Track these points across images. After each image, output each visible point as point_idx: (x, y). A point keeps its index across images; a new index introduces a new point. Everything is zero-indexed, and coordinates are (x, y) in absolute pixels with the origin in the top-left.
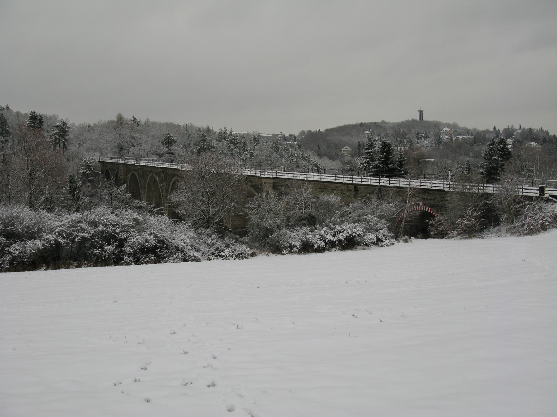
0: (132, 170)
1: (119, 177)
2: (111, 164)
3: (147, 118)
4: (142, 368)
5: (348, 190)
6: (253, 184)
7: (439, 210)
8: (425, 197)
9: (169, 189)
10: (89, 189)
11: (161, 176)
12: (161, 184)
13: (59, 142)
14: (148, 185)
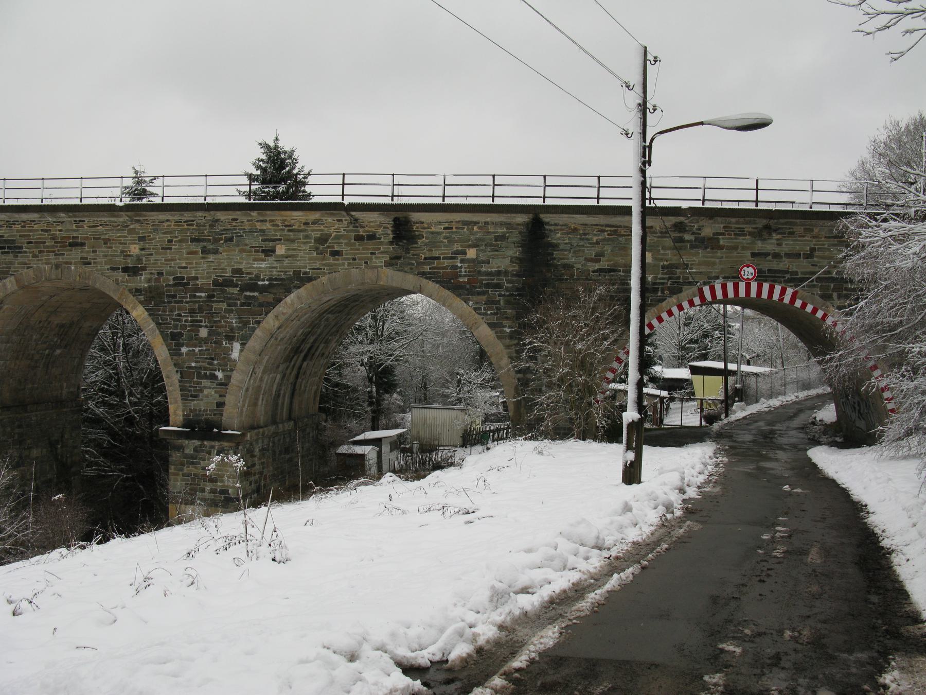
4: (59, 597)
5: (359, 238)
7: (835, 295)
8: (769, 246)
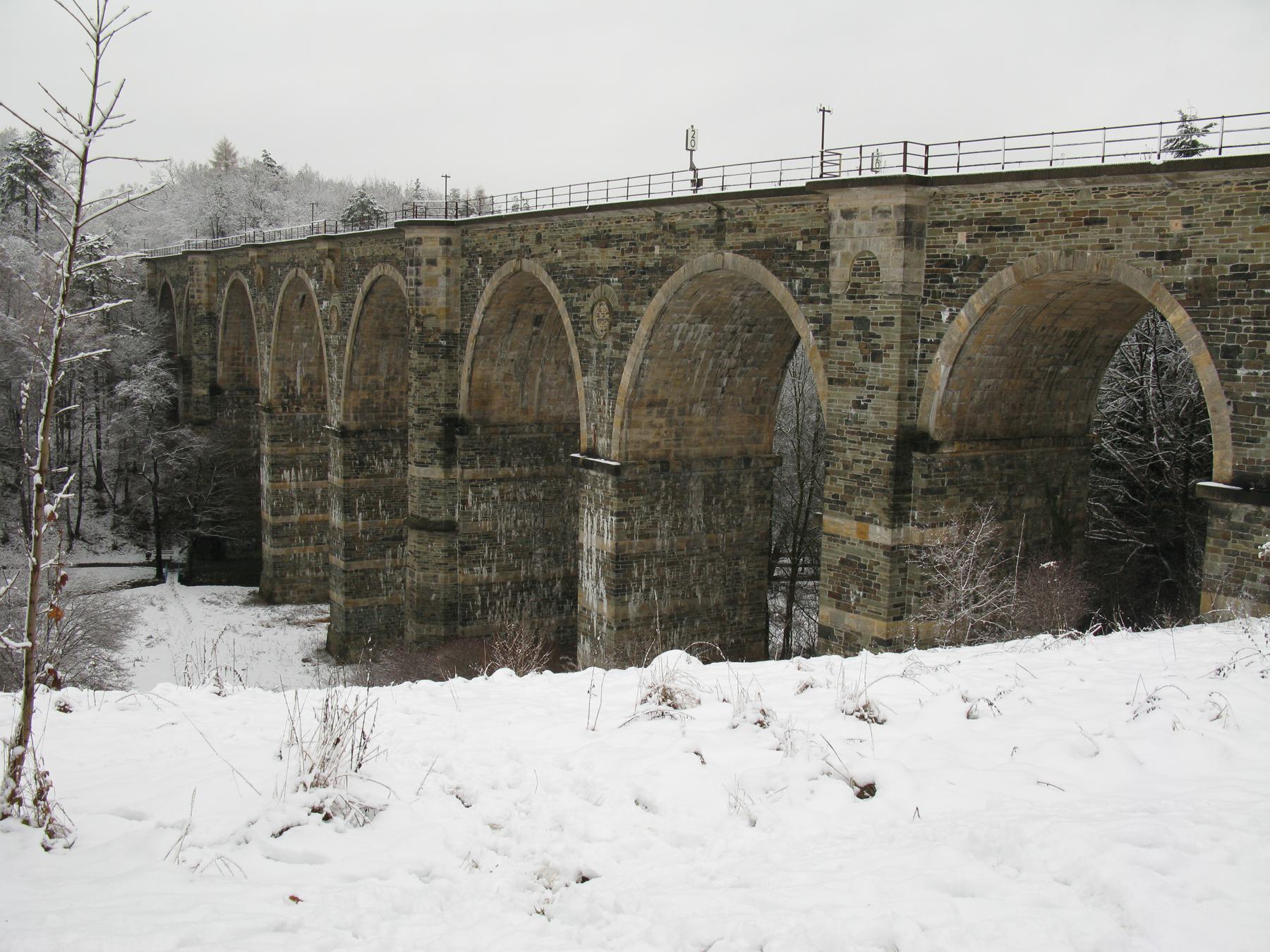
0: (233, 270)
6: (760, 237)
9: (351, 316)
11: (325, 270)
12: (325, 303)
14: (281, 314)
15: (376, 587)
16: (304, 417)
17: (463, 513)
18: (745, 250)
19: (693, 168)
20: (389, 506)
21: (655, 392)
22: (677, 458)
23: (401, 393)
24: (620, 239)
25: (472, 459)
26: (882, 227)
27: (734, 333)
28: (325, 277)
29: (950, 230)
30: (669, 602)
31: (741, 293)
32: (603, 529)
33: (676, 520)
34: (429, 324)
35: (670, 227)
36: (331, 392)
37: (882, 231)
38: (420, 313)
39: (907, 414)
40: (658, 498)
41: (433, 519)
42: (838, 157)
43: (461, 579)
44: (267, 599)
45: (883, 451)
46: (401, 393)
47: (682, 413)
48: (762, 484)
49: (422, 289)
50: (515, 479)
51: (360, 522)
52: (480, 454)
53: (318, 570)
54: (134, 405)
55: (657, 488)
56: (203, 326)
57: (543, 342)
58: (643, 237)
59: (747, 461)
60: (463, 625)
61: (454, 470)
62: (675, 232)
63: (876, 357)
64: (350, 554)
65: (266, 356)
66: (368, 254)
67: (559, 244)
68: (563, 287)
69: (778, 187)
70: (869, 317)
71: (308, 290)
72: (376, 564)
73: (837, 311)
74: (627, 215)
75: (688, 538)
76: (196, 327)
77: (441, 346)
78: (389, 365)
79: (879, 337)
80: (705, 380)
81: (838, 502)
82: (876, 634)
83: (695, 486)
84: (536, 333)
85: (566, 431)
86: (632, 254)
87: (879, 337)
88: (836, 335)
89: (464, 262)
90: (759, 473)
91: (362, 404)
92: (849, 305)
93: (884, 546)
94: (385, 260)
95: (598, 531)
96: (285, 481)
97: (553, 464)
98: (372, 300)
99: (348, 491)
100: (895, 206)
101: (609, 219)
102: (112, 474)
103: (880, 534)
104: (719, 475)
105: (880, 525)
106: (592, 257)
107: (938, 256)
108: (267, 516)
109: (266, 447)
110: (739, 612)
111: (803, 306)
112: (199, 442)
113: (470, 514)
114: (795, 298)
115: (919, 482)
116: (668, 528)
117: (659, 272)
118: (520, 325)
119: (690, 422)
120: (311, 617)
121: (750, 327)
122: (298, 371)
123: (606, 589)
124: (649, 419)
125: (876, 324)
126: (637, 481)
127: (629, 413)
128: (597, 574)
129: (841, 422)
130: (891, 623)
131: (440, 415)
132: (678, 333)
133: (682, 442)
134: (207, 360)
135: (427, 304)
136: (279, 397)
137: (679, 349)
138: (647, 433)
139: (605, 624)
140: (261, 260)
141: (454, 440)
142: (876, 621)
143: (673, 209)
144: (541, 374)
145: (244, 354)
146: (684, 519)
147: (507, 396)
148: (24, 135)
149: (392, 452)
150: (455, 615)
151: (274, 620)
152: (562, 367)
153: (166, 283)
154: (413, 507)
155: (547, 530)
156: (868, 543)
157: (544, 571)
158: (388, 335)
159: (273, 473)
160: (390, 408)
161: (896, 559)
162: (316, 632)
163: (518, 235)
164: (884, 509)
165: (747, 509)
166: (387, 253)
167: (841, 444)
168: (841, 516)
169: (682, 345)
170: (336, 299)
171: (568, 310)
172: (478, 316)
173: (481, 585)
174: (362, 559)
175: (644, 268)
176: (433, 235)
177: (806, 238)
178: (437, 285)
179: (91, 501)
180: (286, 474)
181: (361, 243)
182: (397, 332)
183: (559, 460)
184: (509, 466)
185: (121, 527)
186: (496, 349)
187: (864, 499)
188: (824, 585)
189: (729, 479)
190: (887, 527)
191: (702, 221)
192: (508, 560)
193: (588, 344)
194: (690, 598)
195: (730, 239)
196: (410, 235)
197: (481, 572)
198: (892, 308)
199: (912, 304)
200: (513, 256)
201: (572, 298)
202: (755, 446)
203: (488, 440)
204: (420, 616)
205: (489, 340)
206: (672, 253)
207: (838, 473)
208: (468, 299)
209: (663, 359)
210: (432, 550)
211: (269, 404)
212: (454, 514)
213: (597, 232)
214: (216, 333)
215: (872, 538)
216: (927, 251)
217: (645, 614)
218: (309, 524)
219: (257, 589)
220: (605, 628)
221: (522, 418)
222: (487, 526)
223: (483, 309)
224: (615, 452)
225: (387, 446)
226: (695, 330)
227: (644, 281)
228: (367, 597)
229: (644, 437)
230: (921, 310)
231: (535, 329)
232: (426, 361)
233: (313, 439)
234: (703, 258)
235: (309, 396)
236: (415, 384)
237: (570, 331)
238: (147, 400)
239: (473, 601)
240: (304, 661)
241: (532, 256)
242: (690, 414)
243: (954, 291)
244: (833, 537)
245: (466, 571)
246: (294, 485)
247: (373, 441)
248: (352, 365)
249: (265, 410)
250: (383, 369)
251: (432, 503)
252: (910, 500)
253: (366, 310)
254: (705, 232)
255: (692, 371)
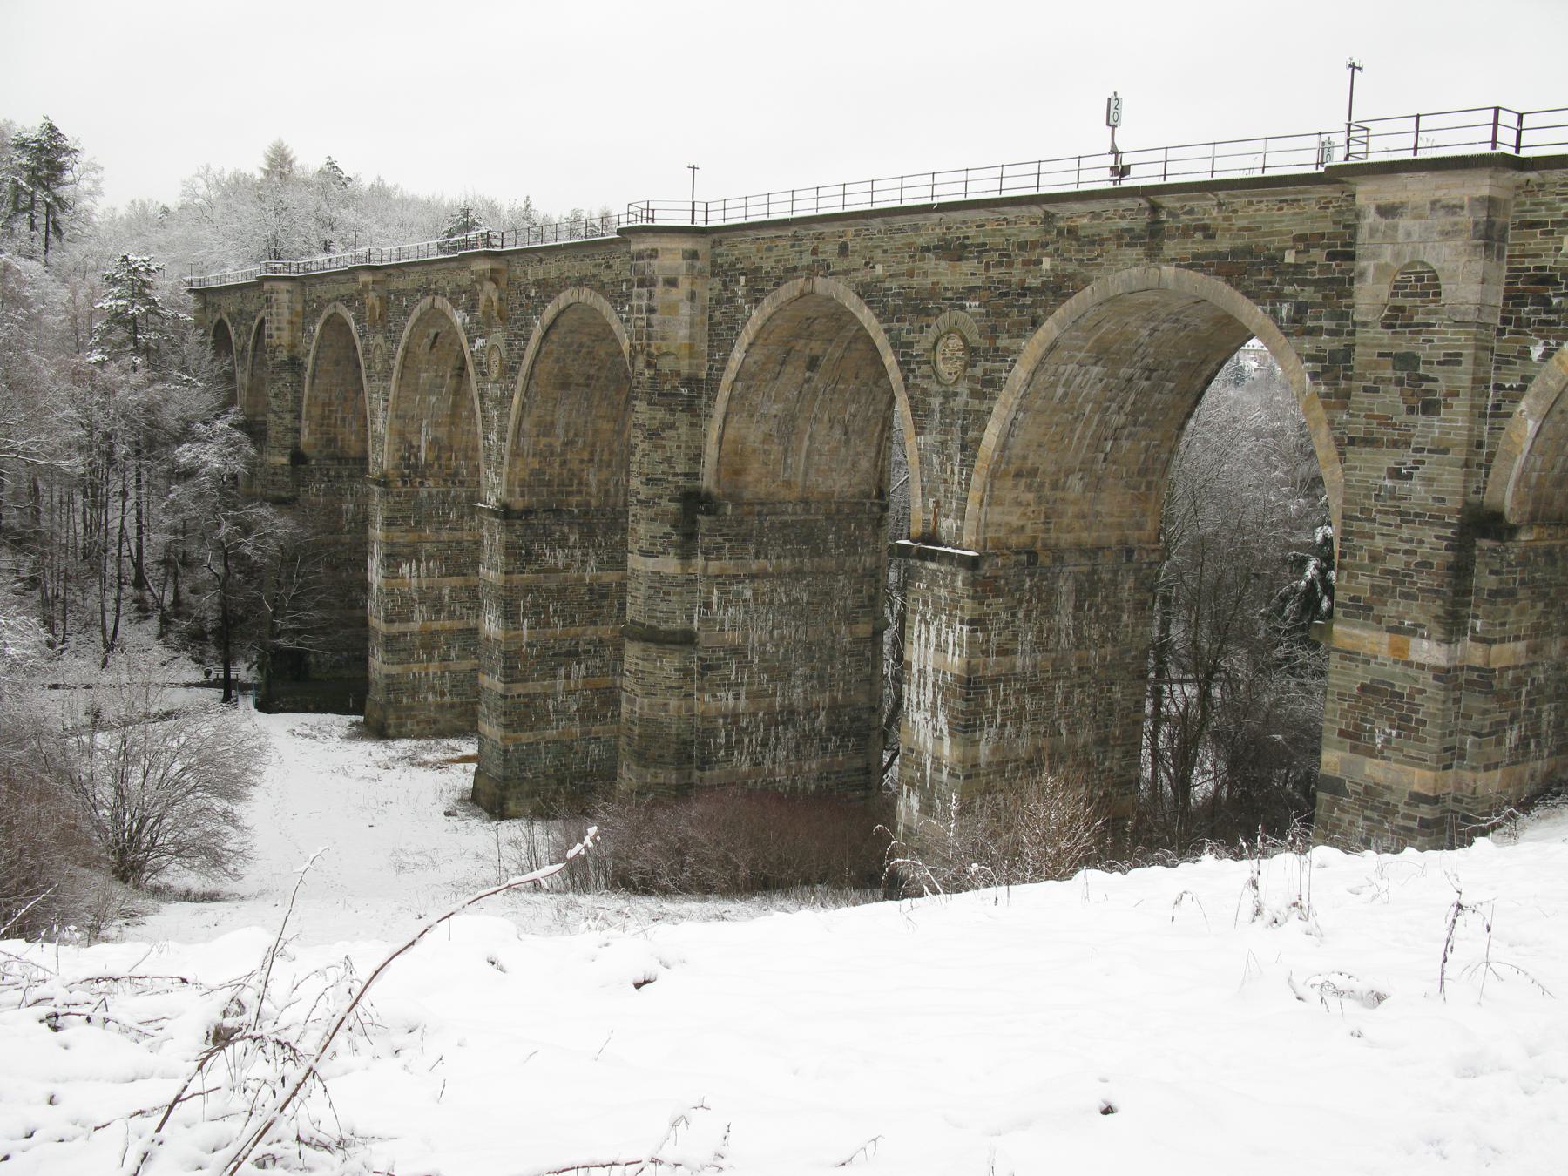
0: (329, 301)
1: (270, 336)
2: (238, 294)
3: (379, 179)
6: (1223, 244)
9: (521, 357)
10: (136, 378)
11: (482, 298)
12: (479, 342)
13: (32, 207)
14: (405, 357)
15: (543, 718)
16: (429, 493)
17: (704, 621)
18: (1197, 263)
19: (1114, 151)
20: (562, 611)
21: (1025, 458)
22: (1046, 547)
23: (582, 461)
24: (982, 248)
25: (719, 548)
26: (1448, 228)
27: (1130, 380)
28: (481, 306)
29: (1552, 232)
30: (1029, 741)
31: (1152, 325)
32: (946, 642)
33: (1041, 631)
34: (665, 365)
35: (1069, 232)
36: (488, 458)
37: (1447, 233)
38: (653, 350)
39: (1473, 487)
40: (1020, 601)
41: (664, 627)
42: (1365, 133)
43: (699, 708)
44: (377, 731)
45: (1437, 537)
46: (582, 461)
47: (1054, 487)
48: (1143, 583)
49: (655, 318)
50: (772, 575)
51: (525, 631)
52: (731, 540)
53: (443, 695)
54: (200, 476)
55: (1020, 588)
56: (283, 375)
57: (815, 394)
58: (1022, 246)
59: (1129, 552)
60: (702, 769)
61: (693, 562)
62: (1077, 239)
63: (1430, 407)
64: (511, 673)
65: (380, 413)
66: (553, 275)
67: (878, 254)
68: (883, 314)
69: (1261, 175)
70: (1419, 353)
71: (452, 326)
72: (543, 686)
73: (1364, 345)
74: (996, 216)
75: (1053, 655)
76: (274, 376)
77: (682, 395)
78: (568, 424)
79: (1435, 380)
80: (1086, 442)
81: (1359, 607)
82: (1416, 788)
83: (1065, 586)
84: (808, 381)
85: (839, 511)
86: (1003, 269)
87: (1435, 380)
88: (1362, 377)
89: (717, 283)
90: (1141, 569)
91: (531, 475)
92: (1386, 336)
93: (1435, 668)
94: (580, 282)
95: (938, 645)
96: (403, 577)
97: (820, 555)
98: (554, 337)
99: (511, 590)
100: (1471, 199)
101: (964, 222)
102: (155, 566)
103: (1428, 651)
104: (1094, 572)
105: (1429, 638)
106: (935, 274)
107: (1528, 269)
108: (377, 622)
109: (377, 532)
110: (1110, 755)
111: (1294, 340)
112: (278, 526)
113: (714, 620)
114: (1281, 328)
115: (1484, 580)
116: (1031, 641)
117: (1049, 293)
118: (789, 369)
119: (1063, 499)
120: (440, 756)
121: (1149, 371)
122: (423, 433)
123: (949, 723)
124: (1013, 495)
125: (1431, 363)
126: (996, 578)
127: (992, 485)
128: (934, 702)
129: (1367, 497)
130: (1440, 773)
131: (678, 488)
132: (1063, 379)
133: (1052, 526)
134: (288, 419)
135: (663, 339)
136: (397, 467)
137: (1061, 401)
138: (1010, 513)
139: (945, 772)
140: (377, 287)
141: (695, 522)
142: (1417, 771)
143: (1077, 207)
144: (810, 436)
145: (337, 411)
146: (1050, 630)
147: (765, 464)
148: (29, 124)
149: (568, 540)
150: (690, 757)
151: (391, 759)
152: (837, 426)
153: (221, 321)
154: (634, 611)
155: (811, 643)
156: (1408, 664)
157: (806, 698)
158: (570, 384)
159: (388, 566)
160: (567, 482)
161: (1451, 686)
162: (451, 776)
163: (808, 245)
164: (1437, 617)
165: (1125, 618)
166: (584, 273)
167: (1367, 527)
168: (1363, 626)
169: (1066, 394)
170: (498, 336)
171: (893, 346)
172: (737, 356)
173: (725, 717)
174: (526, 680)
175: (1023, 288)
176: (674, 246)
177: (1301, 246)
178: (677, 313)
179: (129, 601)
180: (405, 568)
181: (541, 261)
182: (581, 380)
183: (827, 550)
184: (766, 557)
185: (170, 635)
186: (757, 400)
187: (1403, 603)
188: (1331, 721)
189: (1106, 577)
190: (1440, 641)
191: (1124, 224)
192: (760, 683)
193: (925, 392)
194: (1054, 736)
195: (1171, 248)
196: (637, 246)
197: (727, 700)
198: (1459, 340)
199: (1487, 335)
200: (799, 274)
201: (900, 330)
202: (1137, 534)
203: (740, 523)
204: (641, 758)
205: (748, 388)
206: (1071, 268)
207: (1361, 567)
208: (719, 333)
209: (1040, 412)
210: (662, 669)
211: (385, 476)
212: (691, 621)
213: (944, 240)
214: (300, 384)
215: (1414, 657)
216: (1509, 263)
217: (998, 758)
218: (432, 633)
219: (361, 718)
220: (944, 777)
221: (783, 494)
222: (735, 637)
223: (745, 346)
224: (968, 538)
225: (561, 531)
226: (1084, 375)
227: (1024, 306)
228: (531, 730)
229: (1007, 518)
230: (1495, 344)
231: (808, 374)
232: (660, 415)
233: (440, 523)
234: (1125, 274)
235: (436, 466)
236: (641, 446)
237: (895, 375)
238: (218, 469)
239: (715, 737)
240: (447, 814)
241: (832, 274)
242: (1063, 489)
243: (1553, 317)
244: (1349, 655)
245: (707, 698)
246: (414, 582)
247: (545, 525)
248: (520, 424)
249: (378, 483)
250: (560, 430)
251: (663, 606)
252: (1469, 604)
253: (544, 350)
254: (1126, 238)
255: (1072, 431)
